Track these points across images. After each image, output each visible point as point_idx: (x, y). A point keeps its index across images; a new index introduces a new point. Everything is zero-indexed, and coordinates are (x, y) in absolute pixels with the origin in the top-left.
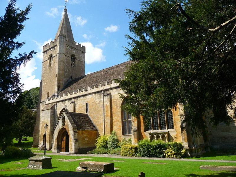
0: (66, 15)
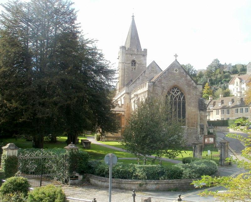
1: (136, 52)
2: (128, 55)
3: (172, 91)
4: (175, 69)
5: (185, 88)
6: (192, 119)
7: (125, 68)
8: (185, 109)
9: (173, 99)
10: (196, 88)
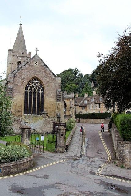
0: (21, 26)
1: (21, 55)
2: (15, 57)
3: (32, 82)
4: (35, 63)
5: (44, 80)
6: (50, 108)
7: (11, 68)
8: (44, 99)
9: (33, 90)
10: (54, 79)
